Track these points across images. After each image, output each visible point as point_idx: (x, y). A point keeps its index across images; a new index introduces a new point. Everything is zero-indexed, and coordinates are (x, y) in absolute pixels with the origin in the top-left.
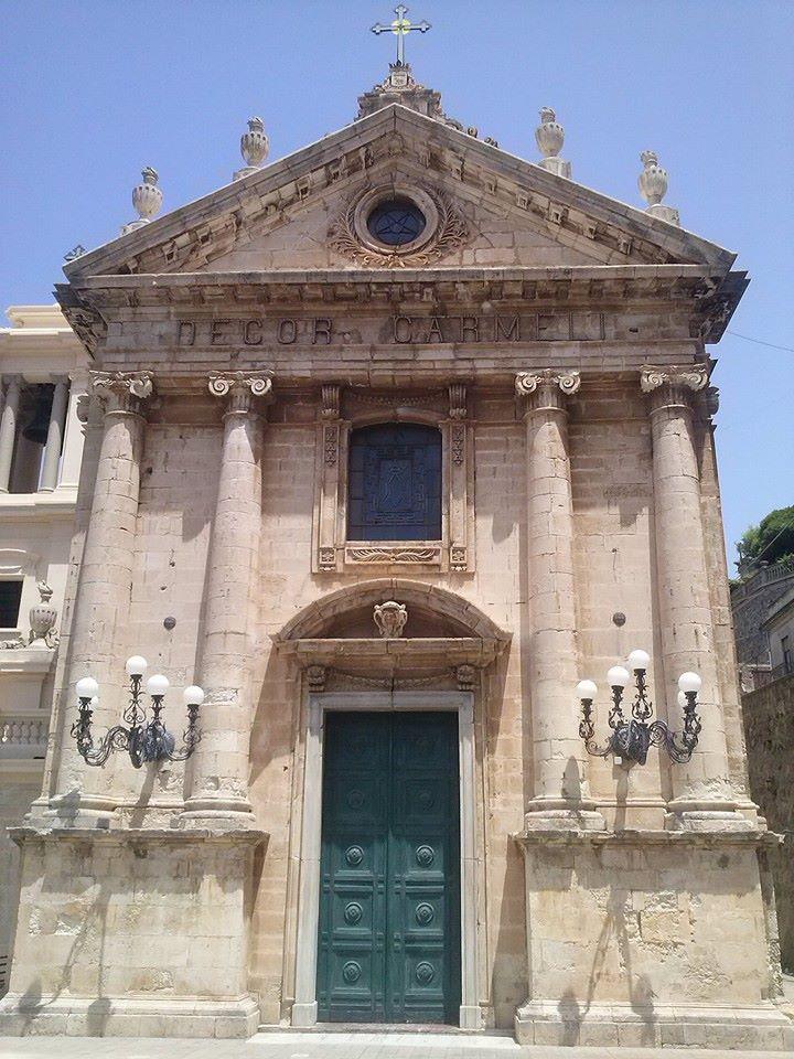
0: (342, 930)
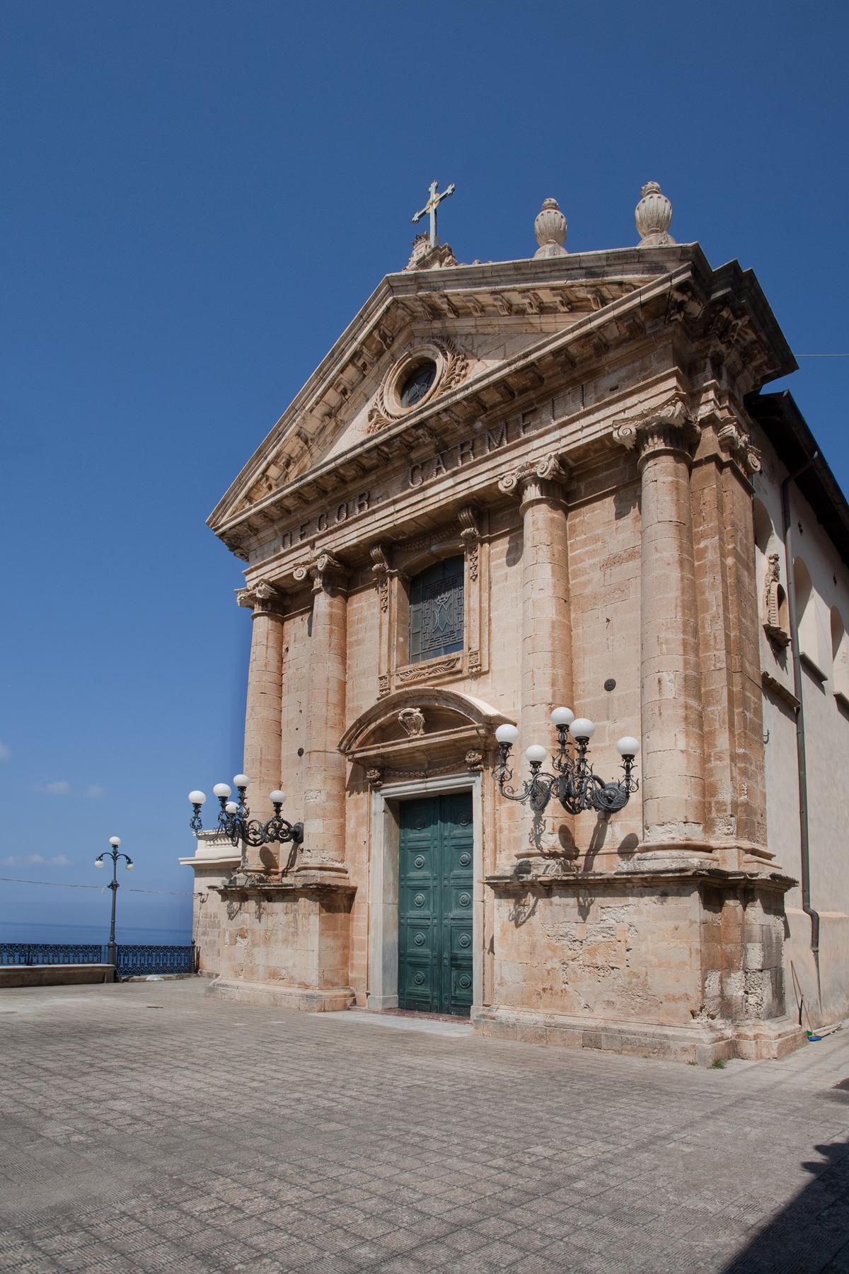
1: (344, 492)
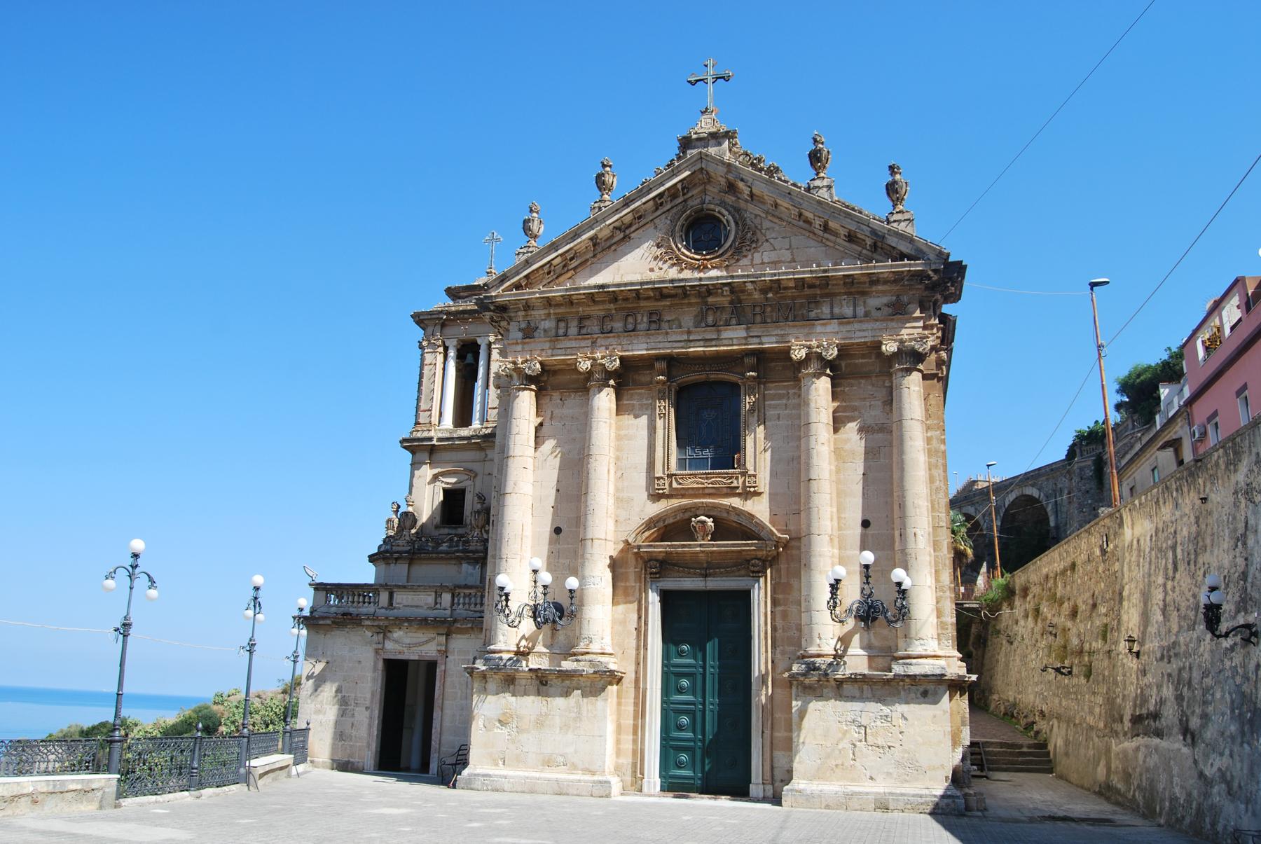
0: (675, 734)
1: (635, 305)
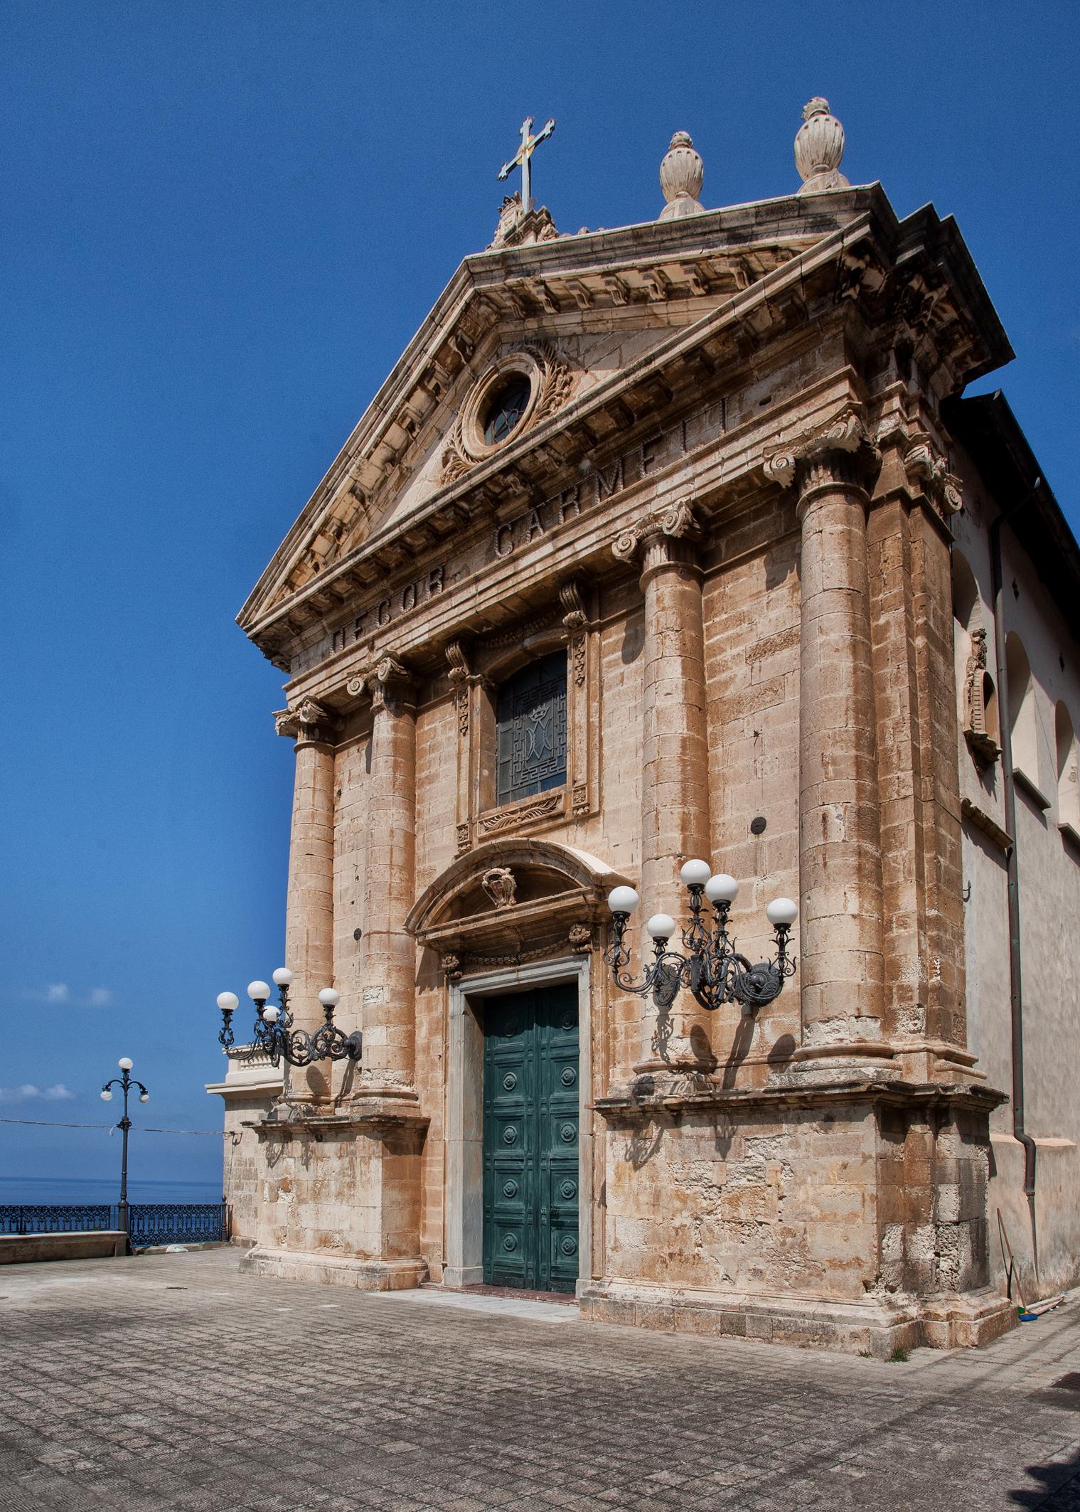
0: (498, 1204)
1: (411, 569)
